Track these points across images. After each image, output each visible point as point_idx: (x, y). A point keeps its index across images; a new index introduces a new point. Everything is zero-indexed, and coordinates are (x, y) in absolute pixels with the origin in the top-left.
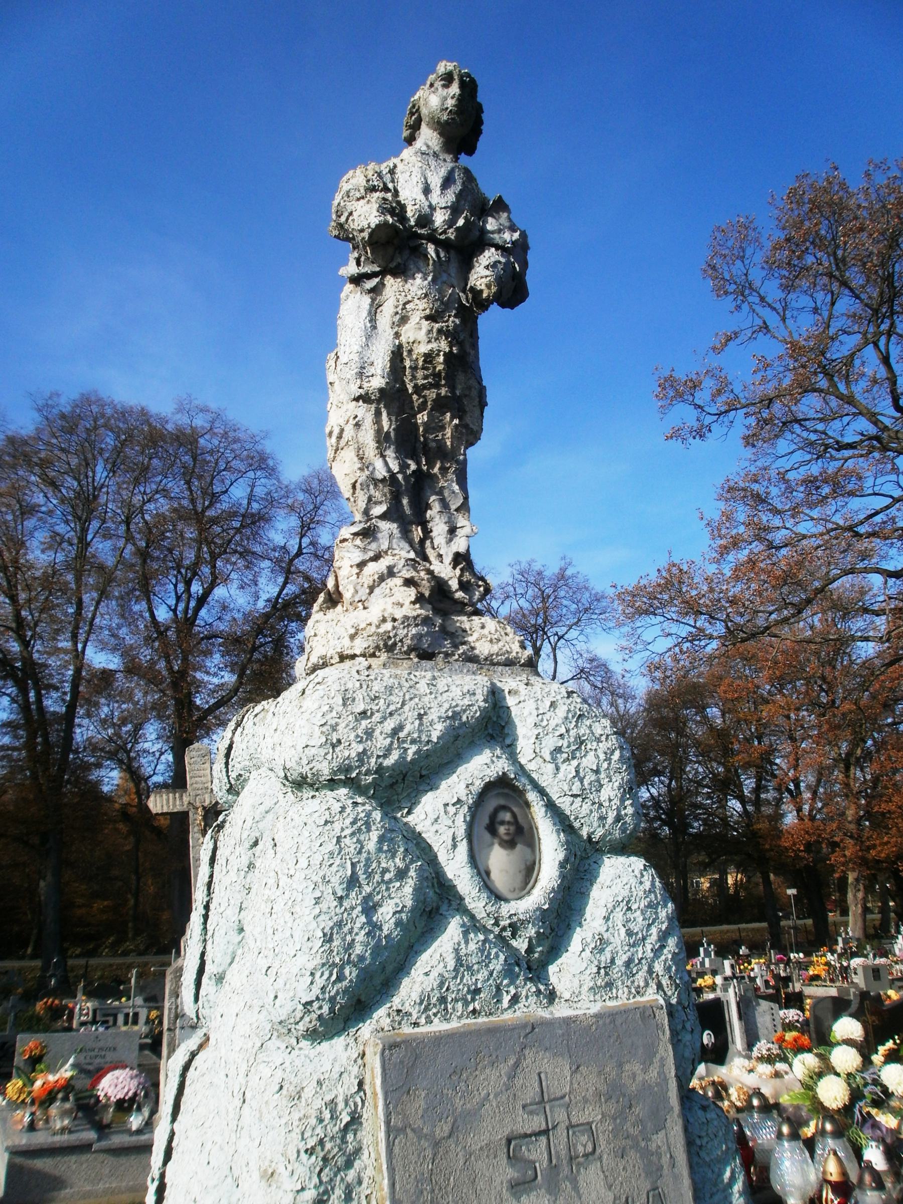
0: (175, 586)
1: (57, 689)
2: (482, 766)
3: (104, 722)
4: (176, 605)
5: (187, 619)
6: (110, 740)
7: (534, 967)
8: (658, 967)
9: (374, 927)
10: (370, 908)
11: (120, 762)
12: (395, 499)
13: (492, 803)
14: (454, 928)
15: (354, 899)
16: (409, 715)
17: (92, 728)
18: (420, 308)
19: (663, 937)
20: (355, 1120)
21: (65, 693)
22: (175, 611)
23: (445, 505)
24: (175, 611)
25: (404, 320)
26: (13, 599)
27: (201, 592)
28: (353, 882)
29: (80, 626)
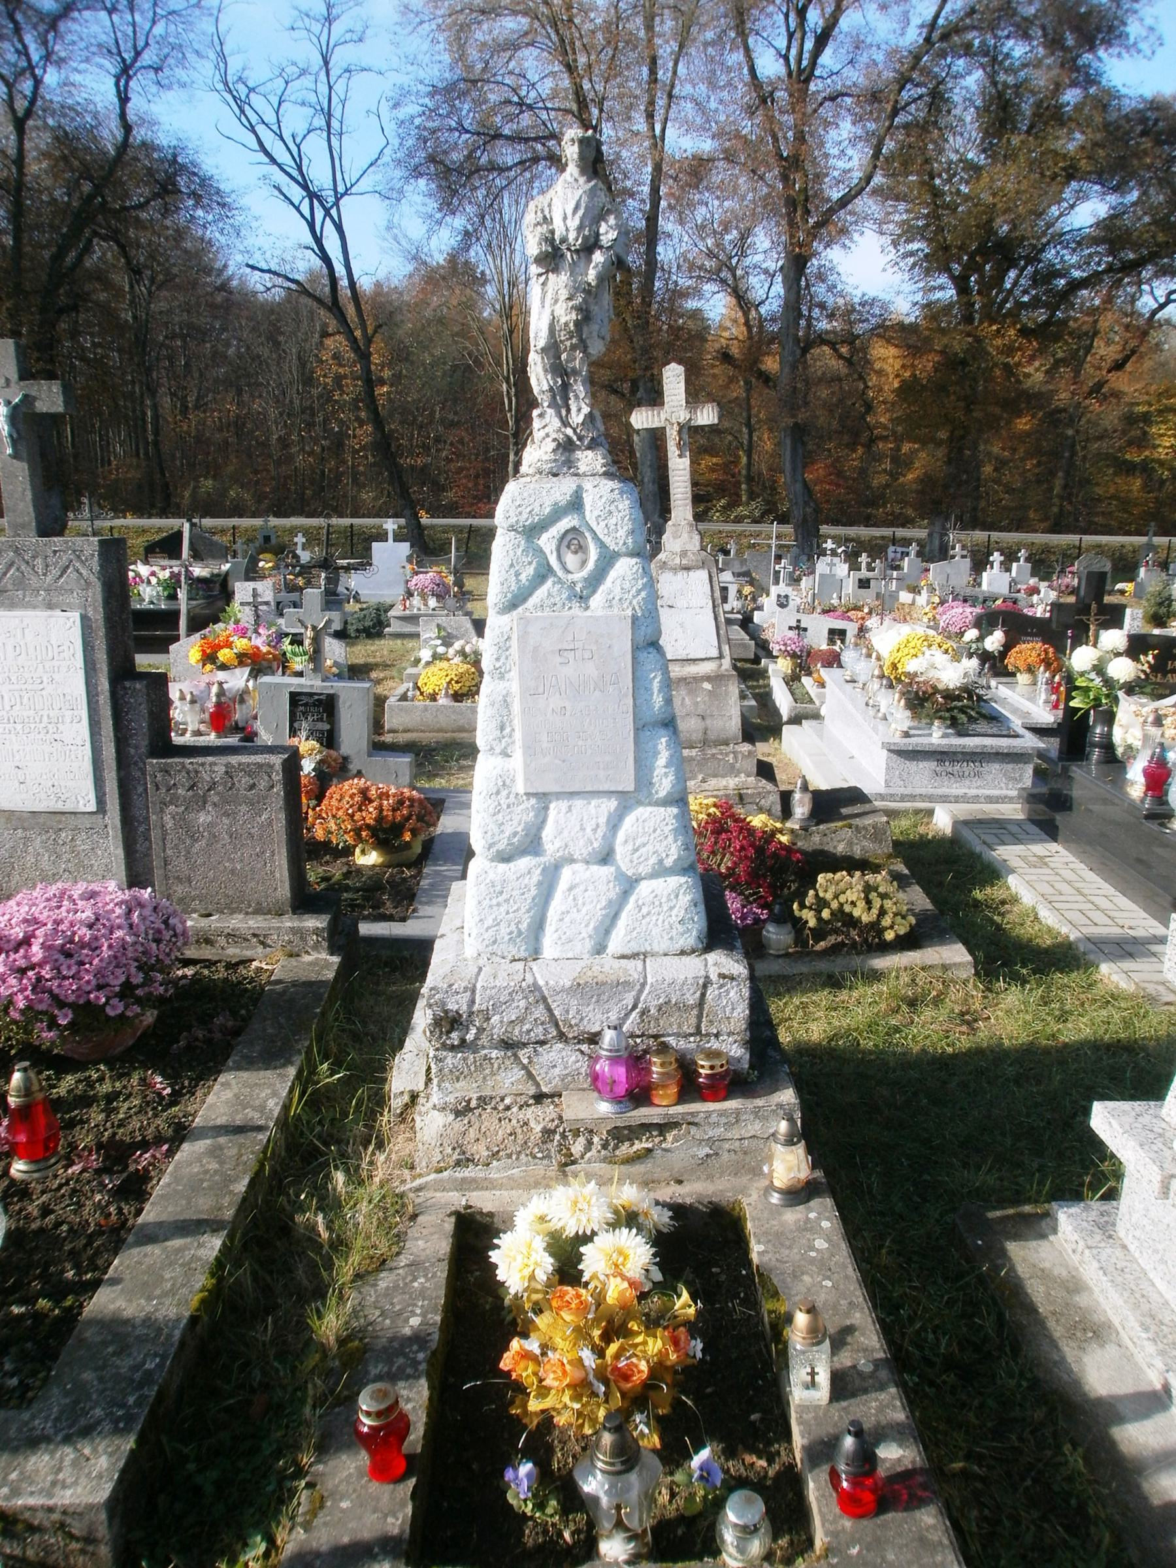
0: (787, 16)
1: (632, 195)
2: (566, 523)
3: (701, 228)
4: (789, 48)
5: (800, 71)
6: (710, 254)
7: (583, 599)
8: (635, 602)
9: (519, 581)
10: (517, 574)
11: (723, 281)
12: (554, 397)
13: (569, 537)
14: (549, 583)
15: (512, 571)
16: (537, 504)
17: (686, 238)
18: (564, 294)
19: (639, 592)
20: (509, 638)
21: (643, 201)
22: (786, 58)
23: (577, 397)
24: (786, 58)
25: (556, 301)
26: (570, 68)
27: (821, 22)
28: (512, 565)
29: (658, 95)
